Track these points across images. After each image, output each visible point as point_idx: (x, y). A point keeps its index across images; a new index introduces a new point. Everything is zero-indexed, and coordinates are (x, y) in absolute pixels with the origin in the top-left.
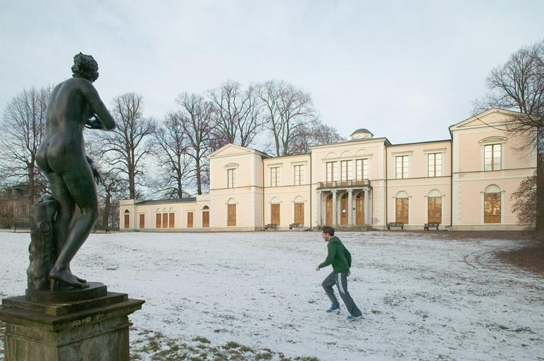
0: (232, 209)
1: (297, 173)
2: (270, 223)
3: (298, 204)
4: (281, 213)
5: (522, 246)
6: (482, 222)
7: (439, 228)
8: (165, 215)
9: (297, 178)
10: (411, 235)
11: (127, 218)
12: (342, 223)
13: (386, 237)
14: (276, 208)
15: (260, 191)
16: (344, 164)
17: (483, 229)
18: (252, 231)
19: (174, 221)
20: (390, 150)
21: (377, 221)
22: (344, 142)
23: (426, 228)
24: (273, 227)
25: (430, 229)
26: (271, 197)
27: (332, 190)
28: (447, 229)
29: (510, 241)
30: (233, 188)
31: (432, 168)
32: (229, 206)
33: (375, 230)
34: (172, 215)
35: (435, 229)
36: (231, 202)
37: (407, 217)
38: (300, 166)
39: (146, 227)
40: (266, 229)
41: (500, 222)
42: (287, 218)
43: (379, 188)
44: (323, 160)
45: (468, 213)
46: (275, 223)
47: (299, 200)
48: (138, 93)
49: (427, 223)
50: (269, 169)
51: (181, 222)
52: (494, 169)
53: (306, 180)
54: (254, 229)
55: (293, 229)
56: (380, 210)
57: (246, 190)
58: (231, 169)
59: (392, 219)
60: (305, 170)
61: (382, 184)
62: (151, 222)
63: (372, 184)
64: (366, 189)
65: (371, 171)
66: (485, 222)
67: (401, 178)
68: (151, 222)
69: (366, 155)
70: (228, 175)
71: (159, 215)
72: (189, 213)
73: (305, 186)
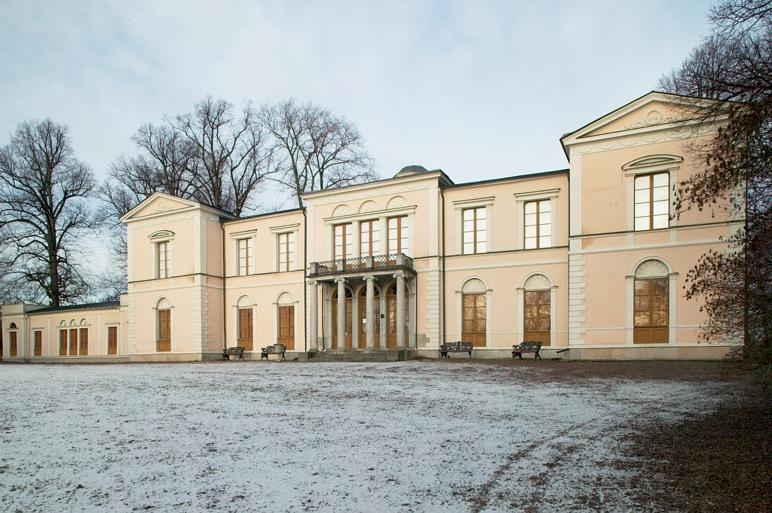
0: (164, 317)
1: (283, 248)
2: (235, 346)
3: (285, 308)
4: (295, 319)
5: (716, 400)
6: (629, 342)
7: (543, 354)
8: (74, 332)
9: (283, 258)
10: (470, 369)
11: (13, 336)
12: (360, 347)
13: (399, 375)
14: (245, 316)
15: (217, 284)
16: (365, 226)
17: (632, 356)
18: (197, 361)
19: (87, 342)
20: (451, 196)
21: (426, 340)
22: (377, 182)
23: (517, 353)
24: (240, 354)
25: (523, 355)
26: (238, 293)
27: (336, 278)
28: (560, 355)
29: (679, 387)
30: (166, 278)
31: (531, 232)
32: (281, 309)
33: (420, 358)
34: (84, 332)
35: (532, 355)
36: (163, 306)
37: (483, 333)
38: (288, 233)
39: (43, 354)
40: (225, 357)
41: (666, 340)
42: (265, 334)
43: (428, 273)
44: (326, 220)
45: (596, 323)
46: (242, 346)
47: (285, 301)
48: (57, 121)
49: (520, 340)
50: (235, 242)
51: (98, 345)
52: (655, 227)
53: (297, 263)
54: (200, 358)
55: (270, 357)
56: (432, 320)
57: (185, 282)
58: (161, 242)
59: (455, 335)
60: (296, 239)
61: (434, 264)
62: (51, 347)
63: (417, 266)
64: (399, 275)
65: (416, 240)
66: (635, 343)
67: (472, 252)
68: (51, 347)
69: (403, 209)
70: (334, 236)
71: (63, 333)
72: (110, 328)
73: (256, 277)
